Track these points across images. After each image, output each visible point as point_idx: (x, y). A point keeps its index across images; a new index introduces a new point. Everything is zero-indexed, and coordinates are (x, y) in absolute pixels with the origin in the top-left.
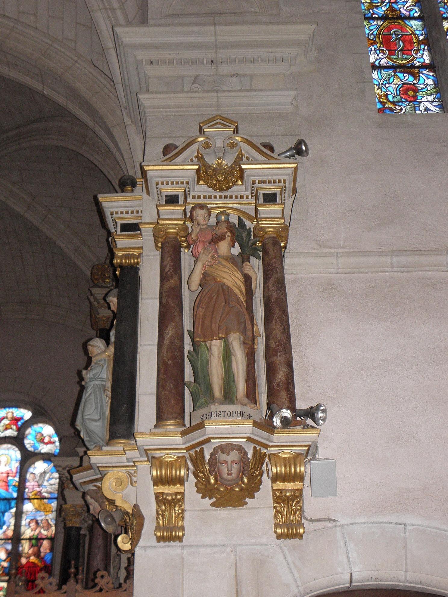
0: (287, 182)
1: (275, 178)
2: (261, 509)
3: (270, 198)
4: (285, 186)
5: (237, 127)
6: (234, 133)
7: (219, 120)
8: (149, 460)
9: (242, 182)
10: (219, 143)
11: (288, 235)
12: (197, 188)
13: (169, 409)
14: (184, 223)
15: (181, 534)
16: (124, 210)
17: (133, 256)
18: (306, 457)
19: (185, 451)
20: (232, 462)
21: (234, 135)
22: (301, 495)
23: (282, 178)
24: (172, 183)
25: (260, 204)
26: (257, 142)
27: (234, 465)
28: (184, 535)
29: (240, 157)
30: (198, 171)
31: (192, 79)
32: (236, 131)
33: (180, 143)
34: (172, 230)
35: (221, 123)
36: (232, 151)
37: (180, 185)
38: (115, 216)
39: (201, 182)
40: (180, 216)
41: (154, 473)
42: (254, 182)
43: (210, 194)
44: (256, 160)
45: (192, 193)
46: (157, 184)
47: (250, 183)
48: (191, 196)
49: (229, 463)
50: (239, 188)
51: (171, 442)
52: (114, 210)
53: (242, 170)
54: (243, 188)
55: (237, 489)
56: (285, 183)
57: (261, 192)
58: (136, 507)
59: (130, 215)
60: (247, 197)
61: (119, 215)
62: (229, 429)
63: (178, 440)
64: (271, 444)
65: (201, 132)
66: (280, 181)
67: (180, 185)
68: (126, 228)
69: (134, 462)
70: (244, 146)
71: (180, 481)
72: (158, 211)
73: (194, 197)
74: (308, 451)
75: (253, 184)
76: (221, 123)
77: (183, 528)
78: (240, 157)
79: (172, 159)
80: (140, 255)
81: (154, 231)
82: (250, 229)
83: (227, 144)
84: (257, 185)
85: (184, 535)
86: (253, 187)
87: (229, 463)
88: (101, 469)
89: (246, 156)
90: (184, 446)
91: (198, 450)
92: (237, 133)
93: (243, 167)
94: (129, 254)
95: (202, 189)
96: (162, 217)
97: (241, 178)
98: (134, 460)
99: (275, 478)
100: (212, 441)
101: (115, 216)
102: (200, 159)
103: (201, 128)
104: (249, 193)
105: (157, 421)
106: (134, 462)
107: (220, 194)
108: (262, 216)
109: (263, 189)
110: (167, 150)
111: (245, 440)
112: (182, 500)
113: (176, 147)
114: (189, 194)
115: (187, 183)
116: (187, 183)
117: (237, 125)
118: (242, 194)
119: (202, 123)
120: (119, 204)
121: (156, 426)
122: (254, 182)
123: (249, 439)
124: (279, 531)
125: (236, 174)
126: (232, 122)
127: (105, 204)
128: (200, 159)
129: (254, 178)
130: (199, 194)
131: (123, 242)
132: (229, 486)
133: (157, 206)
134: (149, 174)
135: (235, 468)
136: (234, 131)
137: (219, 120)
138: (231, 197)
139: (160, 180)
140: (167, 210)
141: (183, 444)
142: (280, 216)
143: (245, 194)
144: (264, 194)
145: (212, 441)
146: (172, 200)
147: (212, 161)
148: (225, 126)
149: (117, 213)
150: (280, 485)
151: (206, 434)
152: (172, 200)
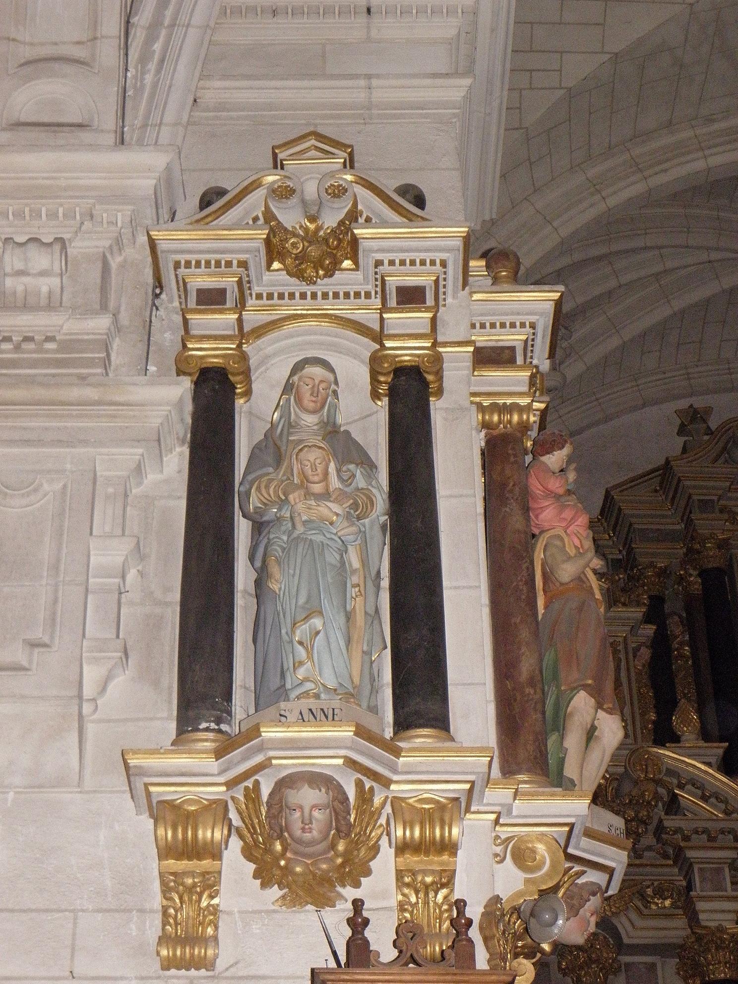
3: (411, 297)
4: (445, 273)
5: (351, 155)
9: (356, 263)
10: (311, 189)
11: (442, 368)
12: (267, 277)
14: (240, 346)
18: (606, 892)
20: (314, 807)
23: (438, 256)
24: (208, 264)
25: (392, 308)
26: (390, 185)
27: (316, 814)
30: (268, 242)
33: (231, 183)
35: (317, 148)
36: (337, 203)
37: (264, 301)
39: (276, 265)
43: (291, 289)
45: (256, 289)
46: (177, 265)
48: (254, 296)
50: (348, 276)
54: (359, 276)
57: (393, 282)
62: (308, 745)
63: (211, 764)
67: (264, 301)
70: (360, 190)
72: (186, 322)
76: (317, 148)
78: (353, 216)
84: (385, 268)
86: (376, 273)
90: (222, 779)
91: (249, 783)
95: (277, 277)
99: (402, 848)
100: (274, 762)
107: (313, 288)
110: (205, 202)
113: (221, 192)
114: (250, 288)
118: (357, 288)
122: (379, 263)
123: (351, 763)
128: (269, 216)
130: (271, 289)
133: (184, 312)
136: (345, 163)
138: (325, 296)
139: (182, 258)
143: (362, 289)
145: (274, 762)
147: (290, 217)
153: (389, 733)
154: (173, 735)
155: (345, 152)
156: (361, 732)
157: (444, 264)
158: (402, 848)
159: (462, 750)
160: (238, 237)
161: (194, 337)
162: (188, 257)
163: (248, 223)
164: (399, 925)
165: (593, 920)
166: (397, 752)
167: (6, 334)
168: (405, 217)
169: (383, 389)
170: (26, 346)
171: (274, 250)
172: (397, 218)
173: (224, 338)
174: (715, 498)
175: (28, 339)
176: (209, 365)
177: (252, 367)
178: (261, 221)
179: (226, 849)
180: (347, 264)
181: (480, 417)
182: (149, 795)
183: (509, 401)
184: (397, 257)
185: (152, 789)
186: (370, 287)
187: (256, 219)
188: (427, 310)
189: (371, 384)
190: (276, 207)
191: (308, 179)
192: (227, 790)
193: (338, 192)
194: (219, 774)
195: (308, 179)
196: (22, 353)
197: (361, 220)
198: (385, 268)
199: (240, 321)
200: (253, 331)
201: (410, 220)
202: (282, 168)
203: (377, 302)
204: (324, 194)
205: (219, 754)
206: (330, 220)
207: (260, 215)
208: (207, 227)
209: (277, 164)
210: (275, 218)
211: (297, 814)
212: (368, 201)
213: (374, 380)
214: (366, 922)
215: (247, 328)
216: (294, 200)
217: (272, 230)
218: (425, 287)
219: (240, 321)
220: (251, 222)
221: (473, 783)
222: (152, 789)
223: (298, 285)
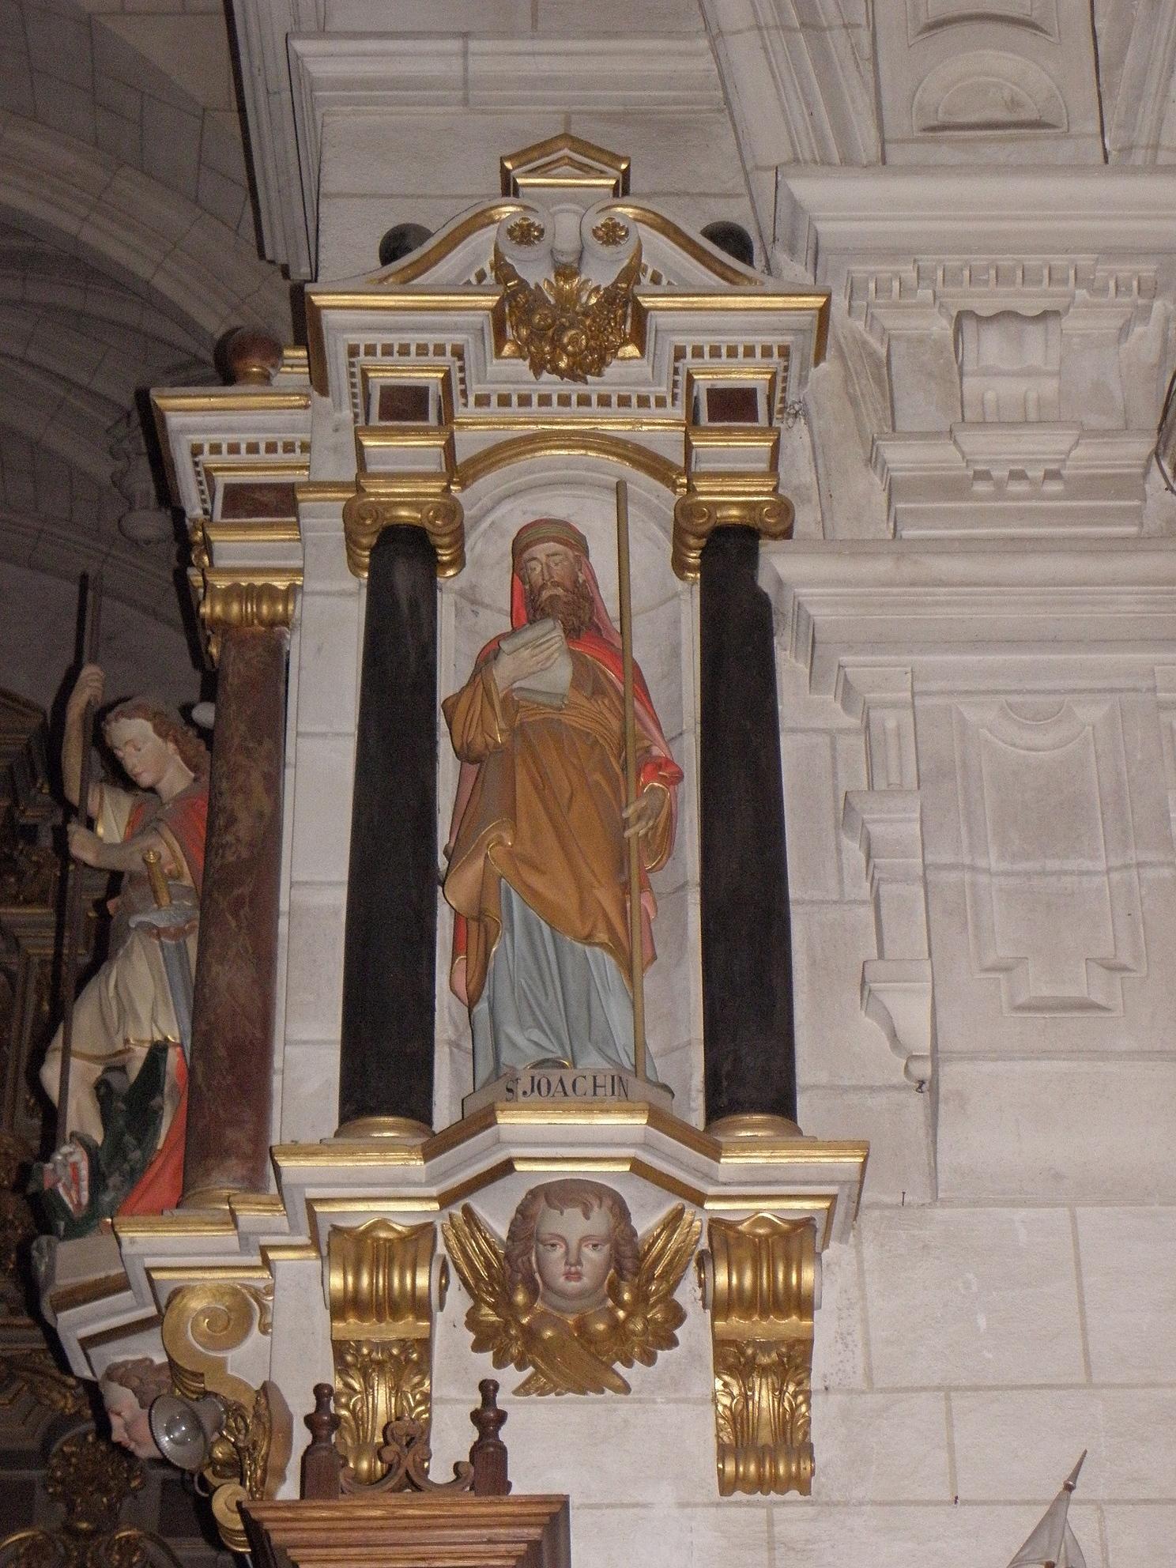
2: (677, 1402)
3: (733, 406)
4: (786, 369)
6: (616, 194)
8: (315, 1244)
10: (566, 229)
12: (494, 366)
13: (385, 1074)
16: (262, 439)
17: (269, 593)
20: (584, 1240)
22: (807, 1356)
27: (588, 1252)
32: (622, 189)
33: (436, 219)
35: (572, 162)
38: (206, 458)
40: (432, 468)
41: (336, 1281)
42: (679, 354)
46: (353, 351)
47: (670, 353)
48: (472, 399)
49: (574, 1244)
51: (384, 1183)
52: (206, 440)
54: (643, 368)
55: (601, 1327)
58: (266, 1389)
59: (244, 457)
61: (225, 459)
64: (711, 1190)
65: (509, 188)
68: (244, 502)
69: (264, 1250)
70: (645, 232)
71: (421, 1307)
72: (360, 448)
74: (830, 1212)
75: (677, 359)
76: (572, 162)
78: (632, 274)
80: (292, 592)
81: (347, 515)
82: (538, 286)
83: (594, 232)
88: (155, 1275)
89: (650, 271)
90: (434, 1191)
93: (647, 302)
94: (251, 586)
95: (509, 370)
96: (372, 468)
97: (639, 337)
98: (266, 1240)
99: (721, 1306)
101: (206, 458)
103: (506, 177)
104: (664, 390)
105: (344, 1119)
106: (264, 1250)
109: (713, 376)
110: (394, 246)
112: (424, 1367)
113: (423, 234)
117: (626, 173)
119: (510, 158)
120: (233, 419)
121: (337, 1134)
123: (639, 1168)
124: (730, 1468)
125: (624, 314)
127: (174, 421)
128: (501, 267)
129: (679, 340)
130: (504, 389)
131: (239, 550)
135: (594, 1258)
136: (615, 188)
137: (566, 152)
138: (604, 401)
139: (362, 339)
141: (429, 1183)
144: (712, 393)
145: (519, 1167)
146: (405, 406)
147: (536, 273)
148: (586, 170)
149: (216, 449)
150: (734, 1324)
152: (405, 406)
153: (697, 1119)
154: (335, 1125)
155: (618, 169)
156: (658, 1119)
157: (785, 352)
158: (721, 1306)
159: (813, 1144)
161: (375, 476)
164: (388, 1424)
166: (715, 1152)
167: (979, 467)
169: (693, 557)
170: (1016, 487)
172: (714, 280)
173: (427, 477)
175: (1018, 476)
176: (397, 521)
177: (467, 525)
178: (490, 278)
179: (442, 1306)
180: (631, 350)
181: (290, 607)
183: (259, 581)
184: (706, 341)
186: (664, 390)
187: (481, 276)
188: (762, 431)
189: (348, 548)
190: (519, 261)
191: (562, 211)
192: (441, 1208)
193: (611, 234)
195: (562, 211)
196: (1006, 500)
197: (646, 280)
199: (450, 449)
200: (473, 462)
201: (731, 282)
202: (516, 194)
203: (679, 412)
205: (427, 1156)
206: (601, 273)
207: (487, 268)
208: (405, 287)
209: (509, 188)
211: (560, 1251)
212: (660, 251)
213: (351, 541)
214: (502, 1417)
215: (460, 458)
216: (539, 249)
217: (509, 297)
218: (426, 389)
219: (450, 449)
220: (474, 281)
221: (833, 1198)
222: (318, 1209)
223: (555, 383)
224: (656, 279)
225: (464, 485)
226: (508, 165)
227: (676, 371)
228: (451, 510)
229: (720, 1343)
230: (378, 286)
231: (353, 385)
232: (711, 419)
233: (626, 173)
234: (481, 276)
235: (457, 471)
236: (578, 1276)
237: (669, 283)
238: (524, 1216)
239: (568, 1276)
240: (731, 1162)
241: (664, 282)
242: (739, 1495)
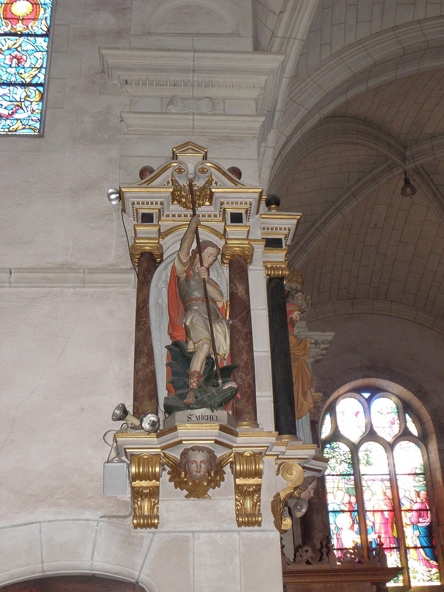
0: (253, 205)
1: (241, 200)
3: (237, 218)
4: (250, 208)
7: (190, 146)
10: (191, 168)
12: (172, 207)
15: (156, 521)
19: (160, 450)
20: (201, 462)
21: (204, 161)
23: (248, 201)
28: (158, 523)
29: (210, 182)
30: (173, 193)
31: (168, 100)
32: (205, 157)
33: (156, 165)
34: (147, 248)
39: (175, 202)
41: (133, 470)
44: (224, 185)
45: (166, 213)
46: (133, 204)
47: (219, 204)
48: (165, 215)
49: (199, 463)
53: (212, 194)
54: (212, 208)
56: (251, 205)
57: (229, 211)
60: (215, 216)
64: (234, 445)
65: (174, 157)
66: (246, 203)
71: (156, 476)
73: (168, 216)
75: (221, 205)
77: (157, 517)
78: (210, 182)
79: (149, 182)
85: (158, 523)
87: (199, 463)
89: (214, 181)
90: (159, 446)
92: (206, 159)
93: (213, 190)
96: (138, 235)
100: (183, 442)
102: (174, 182)
104: (217, 213)
108: (230, 237)
111: (213, 442)
113: (151, 171)
115: (162, 204)
116: (162, 204)
119: (175, 148)
122: (222, 204)
123: (217, 442)
124: (241, 519)
126: (201, 148)
128: (174, 182)
129: (222, 200)
130: (174, 213)
132: (197, 480)
134: (126, 195)
136: (204, 156)
137: (190, 146)
139: (136, 200)
140: (145, 229)
142: (245, 237)
145: (183, 442)
146: (147, 218)
147: (183, 182)
151: (178, 437)
152: (147, 218)
158: (237, 475)
160: (159, 192)
162: (138, 200)
163: (165, 185)
165: (312, 492)
168: (234, 183)
171: (175, 197)
174: (282, 237)
177: (164, 251)
182: (126, 452)
185: (127, 450)
187: (168, 183)
194: (158, 444)
197: (213, 183)
198: (225, 206)
201: (236, 185)
202: (176, 159)
204: (197, 172)
205: (158, 436)
206: (199, 183)
210: (177, 182)
211: (195, 465)
212: (217, 175)
215: (161, 231)
221: (268, 447)
222: (127, 450)
224: (216, 183)
225: (163, 238)
226: (174, 150)
227: (221, 208)
228: (160, 248)
229: (237, 487)
230: (140, 186)
231: (133, 213)
232: (232, 222)
233: (206, 152)
234: (168, 183)
235: (162, 235)
236: (200, 472)
237: (220, 185)
238: (184, 454)
239: (197, 472)
240: (240, 440)
241: (218, 185)
242: (243, 528)
